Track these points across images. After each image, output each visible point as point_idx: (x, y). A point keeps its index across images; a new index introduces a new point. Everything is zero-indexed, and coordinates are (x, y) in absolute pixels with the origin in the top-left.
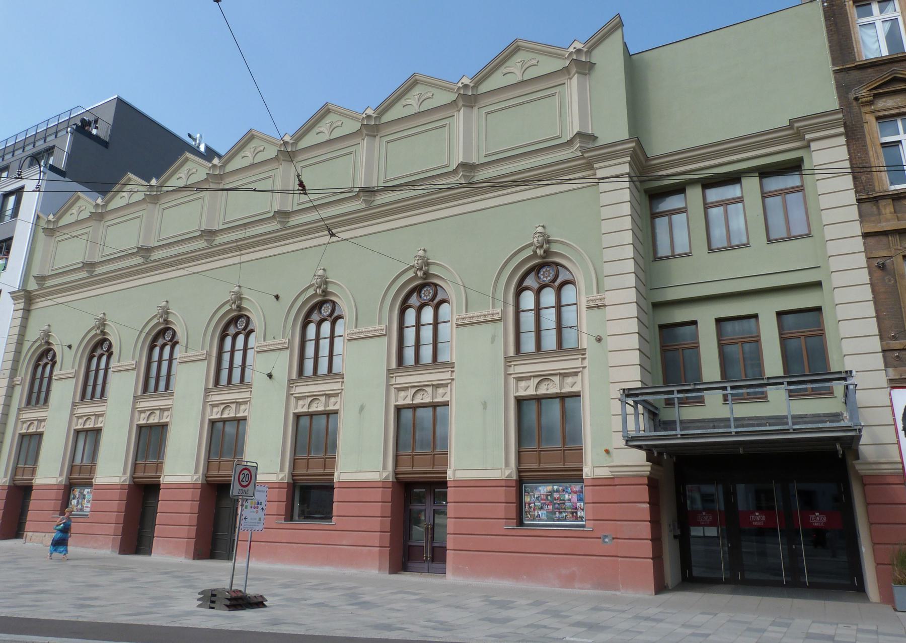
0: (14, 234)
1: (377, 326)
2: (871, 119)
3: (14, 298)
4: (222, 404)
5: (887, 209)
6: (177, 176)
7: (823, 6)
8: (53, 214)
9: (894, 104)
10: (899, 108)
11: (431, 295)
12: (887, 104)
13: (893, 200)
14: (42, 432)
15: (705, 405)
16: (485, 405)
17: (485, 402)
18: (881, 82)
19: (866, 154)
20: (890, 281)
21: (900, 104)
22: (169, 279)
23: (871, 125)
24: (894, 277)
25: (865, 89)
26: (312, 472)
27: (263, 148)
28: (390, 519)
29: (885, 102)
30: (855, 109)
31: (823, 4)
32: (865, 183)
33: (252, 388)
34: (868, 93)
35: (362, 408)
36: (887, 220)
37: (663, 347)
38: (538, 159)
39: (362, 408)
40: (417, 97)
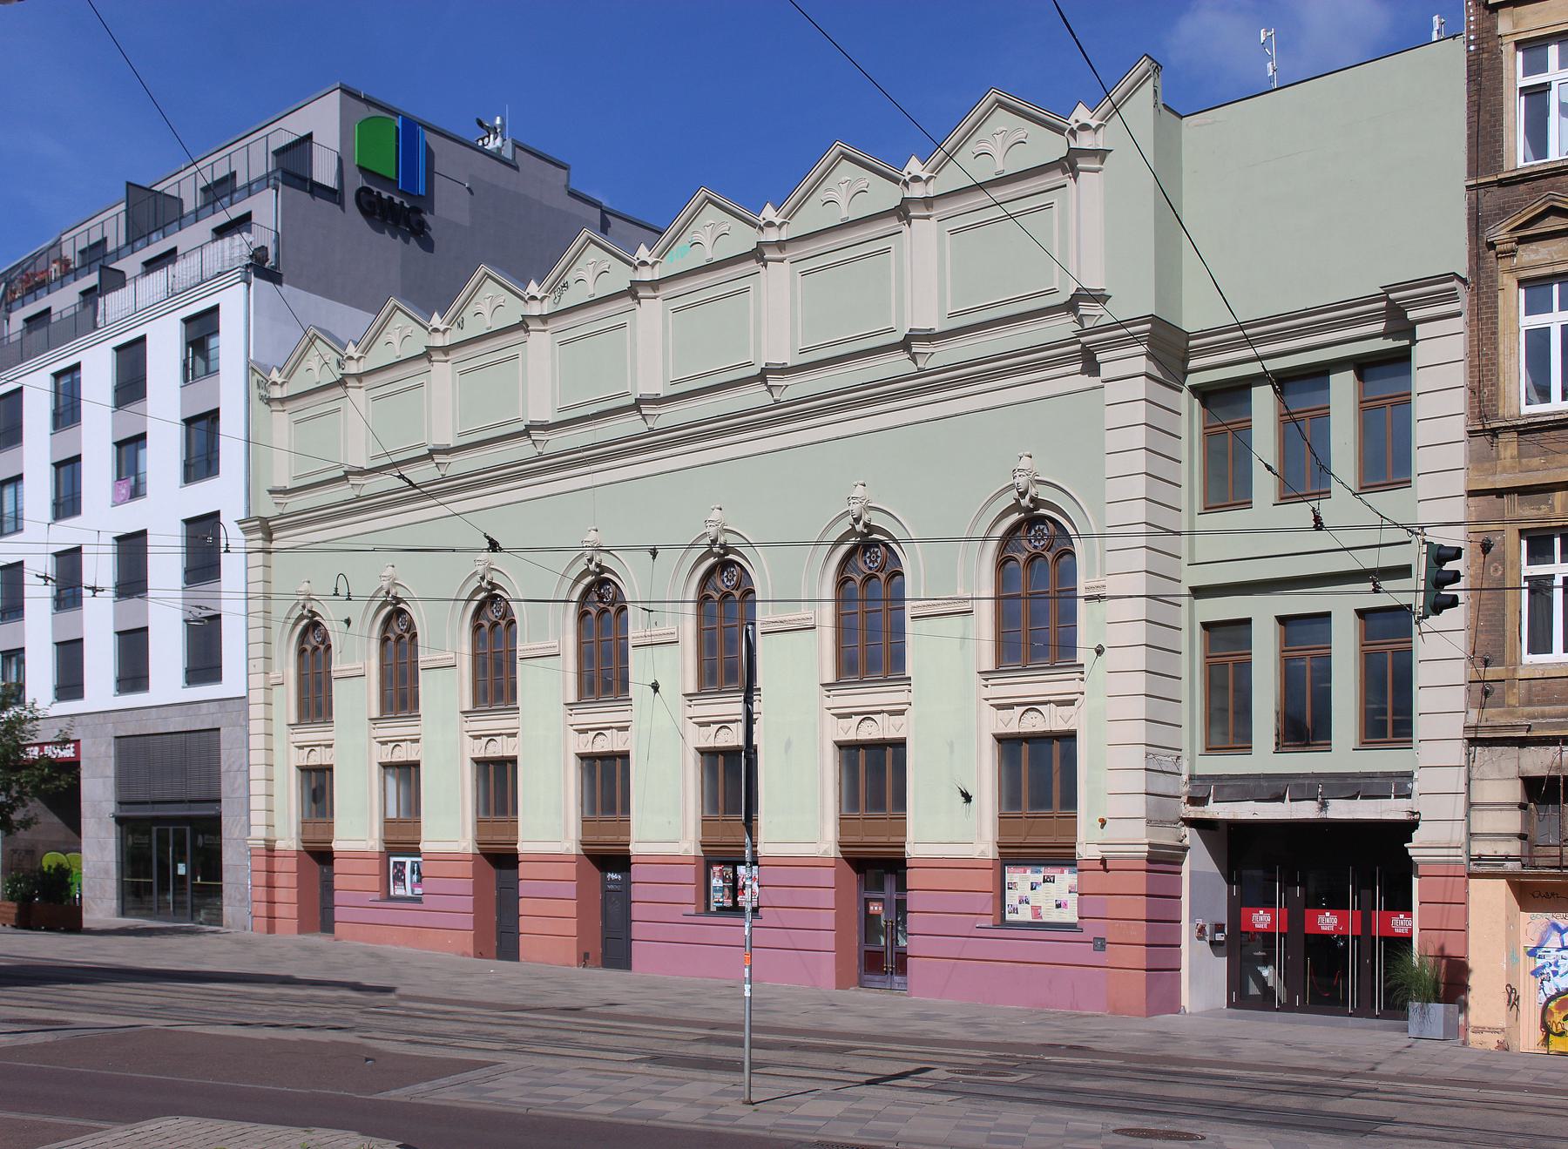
0: (22, 467)
1: (426, 655)
2: (1508, 282)
3: (246, 531)
4: (391, 741)
5: (1508, 447)
6: (821, 195)
7: (1468, 51)
8: (278, 368)
9: (1546, 256)
10: (1552, 264)
11: (879, 560)
12: (1537, 257)
13: (1520, 433)
14: (901, 739)
15: (1412, 748)
16: (951, 745)
17: (952, 742)
18: (1533, 214)
19: (1495, 349)
20: (1496, 569)
21: (1555, 257)
22: (366, 533)
23: (1513, 298)
24: (1503, 564)
25: (1502, 229)
26: (874, 837)
27: (607, 266)
28: (296, 890)
29: (1537, 251)
30: (1491, 262)
31: (1468, 46)
32: (1488, 401)
33: (910, 685)
34: (1508, 236)
35: (788, 744)
36: (1505, 470)
37: (1283, 651)
38: (484, 453)
39: (788, 744)
40: (488, 301)
